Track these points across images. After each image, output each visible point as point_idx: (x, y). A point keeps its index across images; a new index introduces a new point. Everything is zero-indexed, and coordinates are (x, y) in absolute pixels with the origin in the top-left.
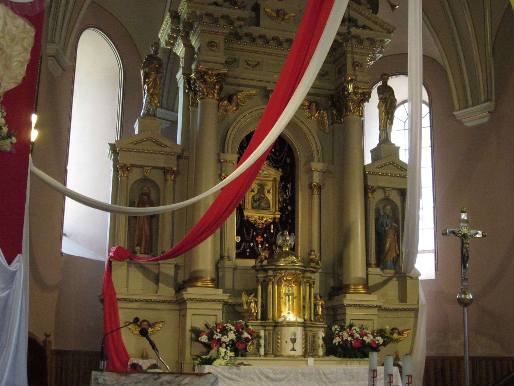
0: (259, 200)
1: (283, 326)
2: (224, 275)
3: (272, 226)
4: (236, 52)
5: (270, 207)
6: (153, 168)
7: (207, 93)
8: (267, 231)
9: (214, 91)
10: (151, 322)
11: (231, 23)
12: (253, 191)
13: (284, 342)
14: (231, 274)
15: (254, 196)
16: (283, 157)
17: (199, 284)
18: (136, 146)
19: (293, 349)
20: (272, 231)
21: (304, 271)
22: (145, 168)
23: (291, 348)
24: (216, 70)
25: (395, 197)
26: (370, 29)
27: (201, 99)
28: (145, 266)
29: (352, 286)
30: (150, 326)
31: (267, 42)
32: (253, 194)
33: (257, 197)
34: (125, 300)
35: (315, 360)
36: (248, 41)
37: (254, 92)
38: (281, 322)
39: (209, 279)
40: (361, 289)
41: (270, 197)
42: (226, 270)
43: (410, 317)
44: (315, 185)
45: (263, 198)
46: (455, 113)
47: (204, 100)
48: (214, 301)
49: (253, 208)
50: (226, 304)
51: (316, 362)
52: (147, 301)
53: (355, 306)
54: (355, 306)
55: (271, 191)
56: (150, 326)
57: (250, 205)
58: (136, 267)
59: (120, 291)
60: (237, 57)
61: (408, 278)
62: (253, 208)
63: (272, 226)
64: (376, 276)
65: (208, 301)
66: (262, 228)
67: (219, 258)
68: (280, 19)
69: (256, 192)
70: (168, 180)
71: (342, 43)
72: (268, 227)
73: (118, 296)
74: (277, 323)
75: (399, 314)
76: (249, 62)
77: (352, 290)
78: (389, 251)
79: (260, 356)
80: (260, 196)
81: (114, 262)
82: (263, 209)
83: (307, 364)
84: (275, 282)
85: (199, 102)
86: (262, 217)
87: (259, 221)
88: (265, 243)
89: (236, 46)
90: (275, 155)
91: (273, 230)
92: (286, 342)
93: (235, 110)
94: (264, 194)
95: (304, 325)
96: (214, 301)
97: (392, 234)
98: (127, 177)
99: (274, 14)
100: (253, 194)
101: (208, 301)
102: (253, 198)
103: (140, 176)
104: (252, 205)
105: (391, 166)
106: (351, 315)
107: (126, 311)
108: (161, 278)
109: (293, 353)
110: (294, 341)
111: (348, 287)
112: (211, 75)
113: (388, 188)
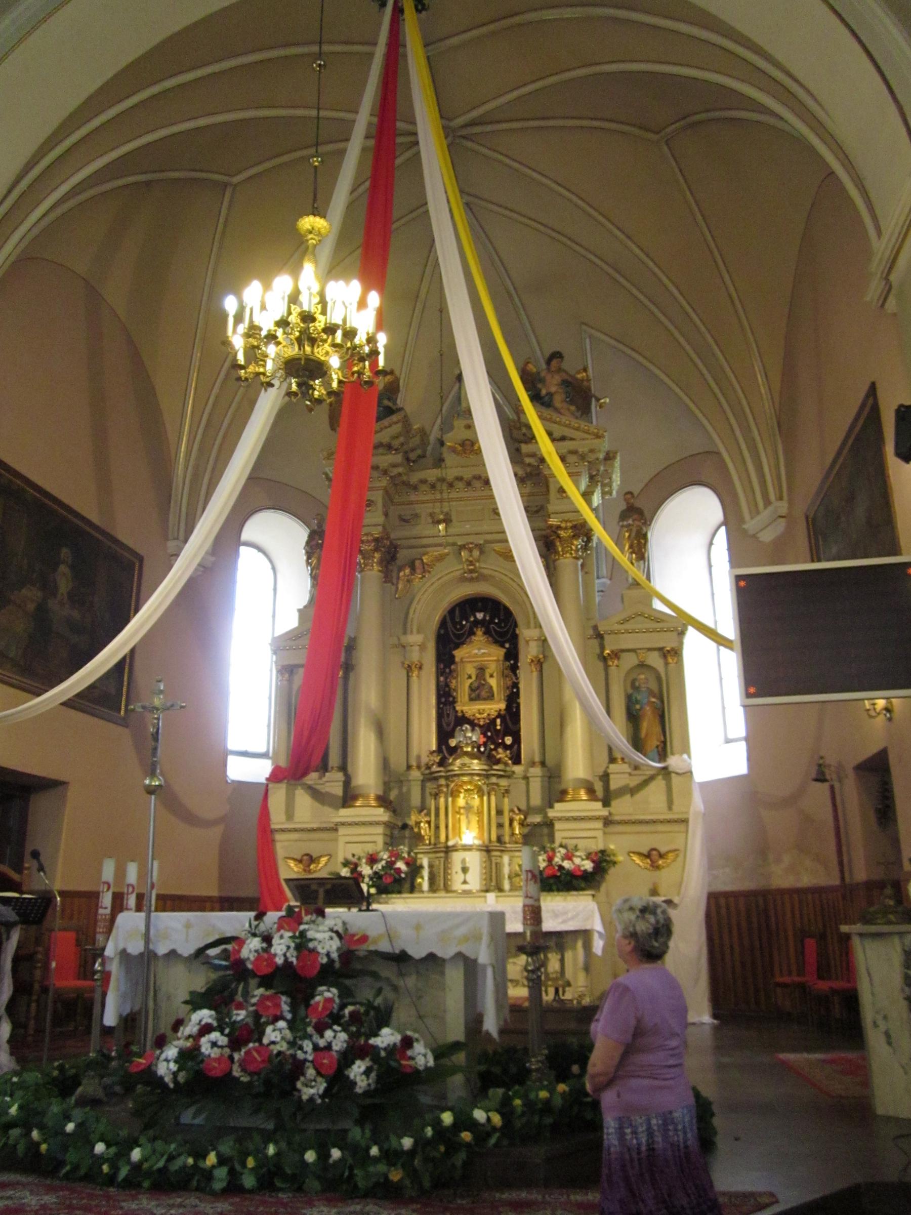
0: (478, 688)
1: (456, 850)
2: (409, 791)
3: (498, 721)
4: (416, 506)
5: (493, 696)
6: (650, 649)
7: (563, 551)
8: (492, 727)
9: (571, 548)
10: (663, 850)
11: (385, 472)
12: (470, 677)
13: (454, 872)
14: (419, 788)
15: (471, 684)
16: (511, 626)
17: (358, 803)
18: (622, 626)
19: (465, 882)
20: (498, 727)
21: (487, 776)
22: (639, 651)
23: (462, 880)
24: (570, 521)
25: (655, 660)
26: (572, 439)
27: (360, 572)
28: (314, 786)
29: (570, 791)
30: (661, 856)
31: (451, 485)
32: (470, 681)
33: (476, 685)
34: (283, 830)
35: (497, 897)
36: (427, 489)
37: (446, 551)
38: (453, 846)
39: (372, 796)
40: (583, 795)
41: (493, 682)
42: (413, 783)
43: (678, 832)
44: (609, 654)
45: (483, 685)
46: (745, 526)
47: (363, 573)
48: (371, 824)
49: (471, 699)
50: (387, 825)
51: (500, 899)
52: (661, 822)
53: (567, 819)
54: (567, 819)
55: (495, 674)
56: (661, 856)
57: (467, 697)
58: (302, 788)
59: (277, 818)
60: (418, 511)
61: (673, 775)
62: (471, 699)
63: (498, 721)
64: (622, 776)
65: (364, 824)
66: (484, 725)
67: (405, 768)
68: (468, 452)
69: (474, 678)
70: (669, 663)
71: (538, 466)
72: (493, 721)
73: (273, 826)
74: (447, 847)
75: (660, 828)
76: (404, 517)
77: (569, 797)
78: (646, 735)
79: (422, 892)
80: (480, 683)
81: (271, 786)
82: (485, 699)
83: (486, 902)
84: (449, 794)
85: (359, 576)
86: (484, 710)
87: (478, 716)
88: (489, 743)
89: (413, 497)
90: (500, 627)
91: (501, 725)
92: (456, 873)
93: (421, 578)
94: (484, 680)
95: (487, 850)
96: (371, 824)
97: (649, 713)
98: (617, 666)
99: (460, 448)
100: (470, 681)
101: (364, 824)
102: (470, 687)
103: (636, 662)
104: (470, 695)
105: (640, 618)
106: (562, 832)
107: (286, 844)
108: (341, 801)
109: (466, 887)
110: (465, 870)
111: (564, 792)
112: (566, 528)
113: (640, 649)
